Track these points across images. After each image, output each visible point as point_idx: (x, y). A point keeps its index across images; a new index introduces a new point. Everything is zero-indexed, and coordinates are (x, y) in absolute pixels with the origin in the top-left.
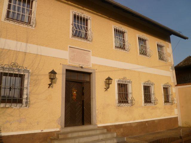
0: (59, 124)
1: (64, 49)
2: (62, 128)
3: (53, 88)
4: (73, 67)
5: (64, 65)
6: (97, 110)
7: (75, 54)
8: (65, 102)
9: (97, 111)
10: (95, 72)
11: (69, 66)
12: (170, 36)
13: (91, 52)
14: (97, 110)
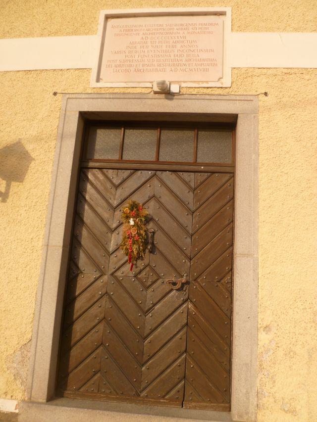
0: (17, 376)
1: (79, 28)
2: (30, 402)
3: (9, 200)
4: (124, 96)
5: (69, 97)
6: (267, 328)
7: (138, 39)
8: (59, 288)
9: (264, 338)
10: (255, 112)
11: (99, 95)
12: (12, 182)
13: (229, 14)
14: (267, 328)
